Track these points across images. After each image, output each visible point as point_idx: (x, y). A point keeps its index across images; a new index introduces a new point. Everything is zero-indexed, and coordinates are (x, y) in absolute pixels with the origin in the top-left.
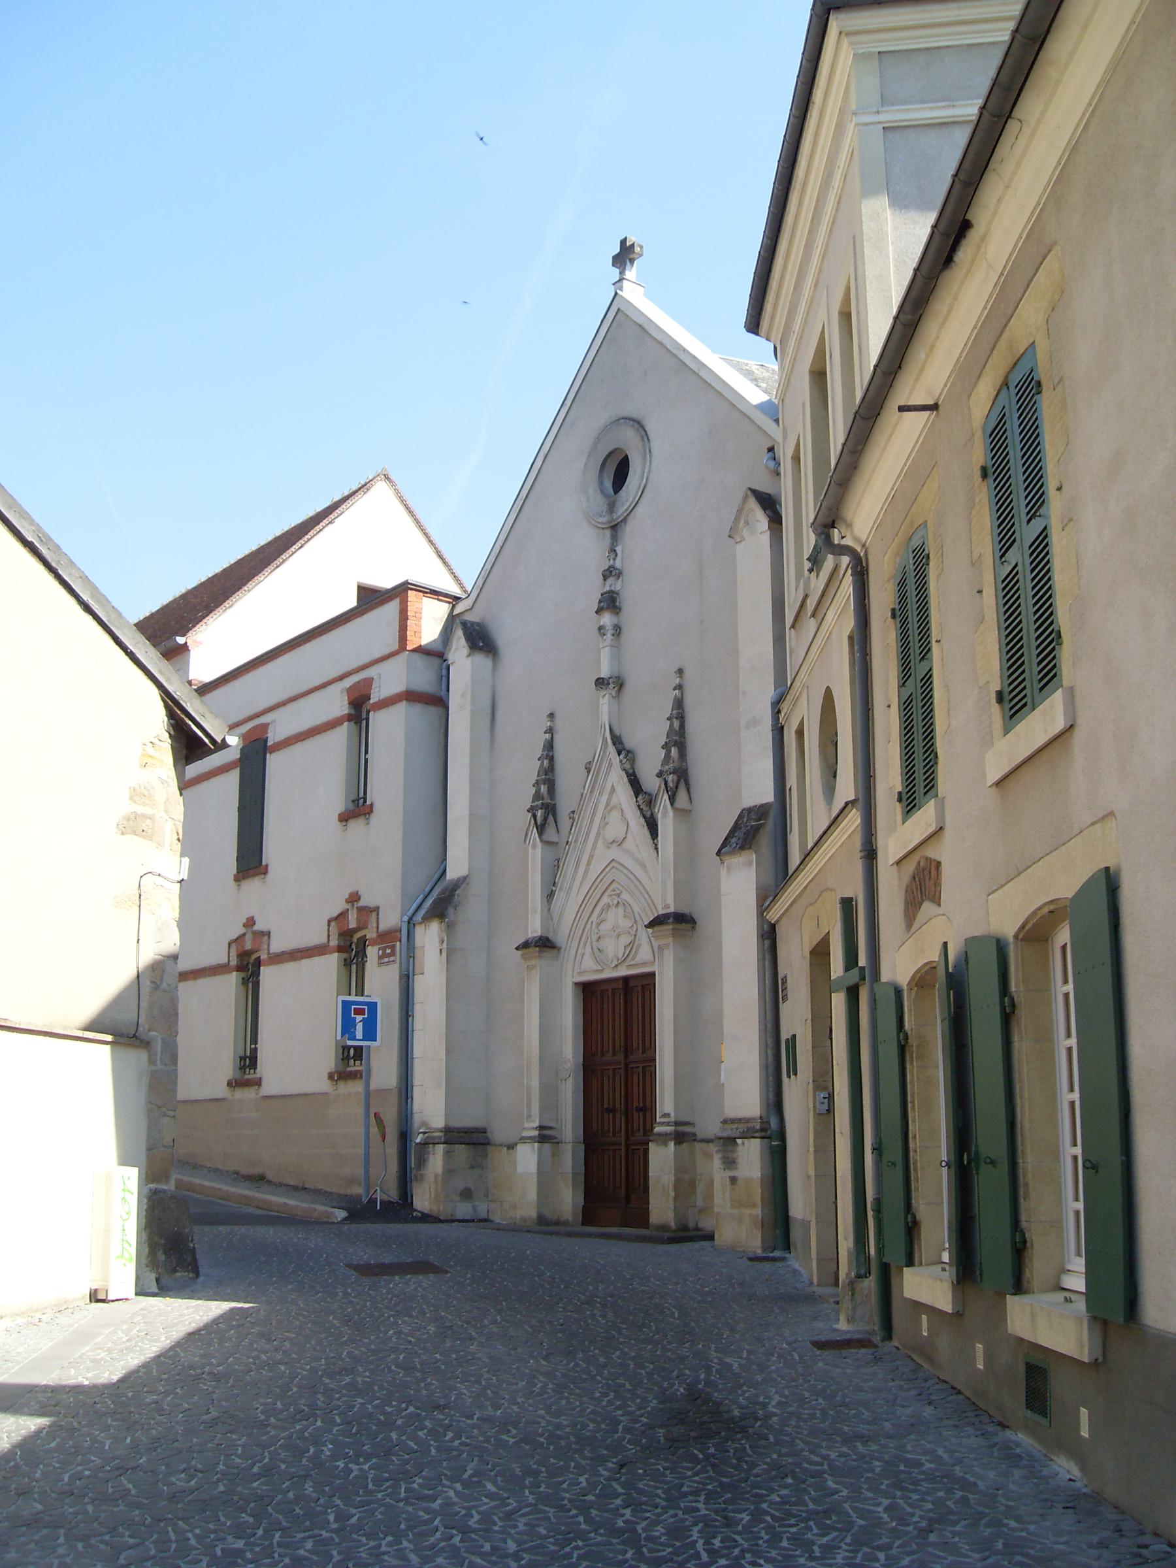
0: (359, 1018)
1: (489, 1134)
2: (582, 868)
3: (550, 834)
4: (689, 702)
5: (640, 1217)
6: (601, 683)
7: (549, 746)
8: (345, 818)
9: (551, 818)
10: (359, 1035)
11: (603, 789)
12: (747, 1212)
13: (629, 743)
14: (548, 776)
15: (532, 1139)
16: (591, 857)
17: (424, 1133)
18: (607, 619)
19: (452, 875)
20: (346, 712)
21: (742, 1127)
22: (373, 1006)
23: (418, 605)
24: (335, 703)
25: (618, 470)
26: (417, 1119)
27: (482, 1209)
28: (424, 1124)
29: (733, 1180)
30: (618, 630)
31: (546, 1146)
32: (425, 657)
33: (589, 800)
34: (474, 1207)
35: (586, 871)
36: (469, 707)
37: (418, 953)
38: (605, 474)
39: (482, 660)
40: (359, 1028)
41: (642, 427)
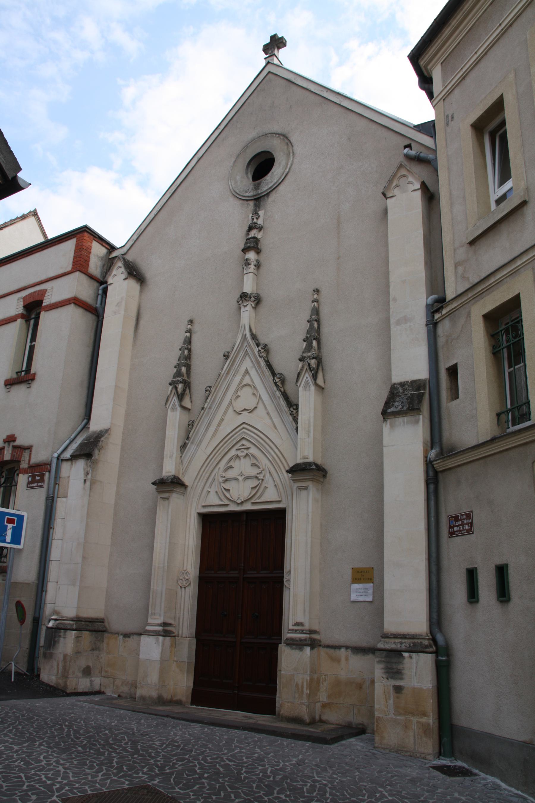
0: (10, 526)
1: (106, 624)
2: (212, 429)
3: (187, 403)
4: (324, 312)
5: (268, 706)
6: (244, 296)
7: (188, 341)
8: (10, 383)
9: (188, 390)
10: (8, 538)
11: (237, 372)
12: (415, 719)
13: (263, 340)
14: (186, 360)
15: (157, 634)
16: (222, 420)
17: (56, 620)
18: (251, 255)
19: (95, 426)
20: (21, 312)
21: (406, 643)
22: (21, 518)
23: (89, 244)
24: (14, 306)
25: (262, 165)
26: (48, 609)
27: (97, 682)
28: (55, 612)
29: (398, 689)
30: (258, 265)
31: (168, 639)
32: (89, 280)
33: (225, 379)
34: (91, 682)
35: (216, 431)
36: (122, 312)
37: (62, 482)
38: (249, 169)
39: (132, 284)
40: (9, 533)
41: (287, 138)
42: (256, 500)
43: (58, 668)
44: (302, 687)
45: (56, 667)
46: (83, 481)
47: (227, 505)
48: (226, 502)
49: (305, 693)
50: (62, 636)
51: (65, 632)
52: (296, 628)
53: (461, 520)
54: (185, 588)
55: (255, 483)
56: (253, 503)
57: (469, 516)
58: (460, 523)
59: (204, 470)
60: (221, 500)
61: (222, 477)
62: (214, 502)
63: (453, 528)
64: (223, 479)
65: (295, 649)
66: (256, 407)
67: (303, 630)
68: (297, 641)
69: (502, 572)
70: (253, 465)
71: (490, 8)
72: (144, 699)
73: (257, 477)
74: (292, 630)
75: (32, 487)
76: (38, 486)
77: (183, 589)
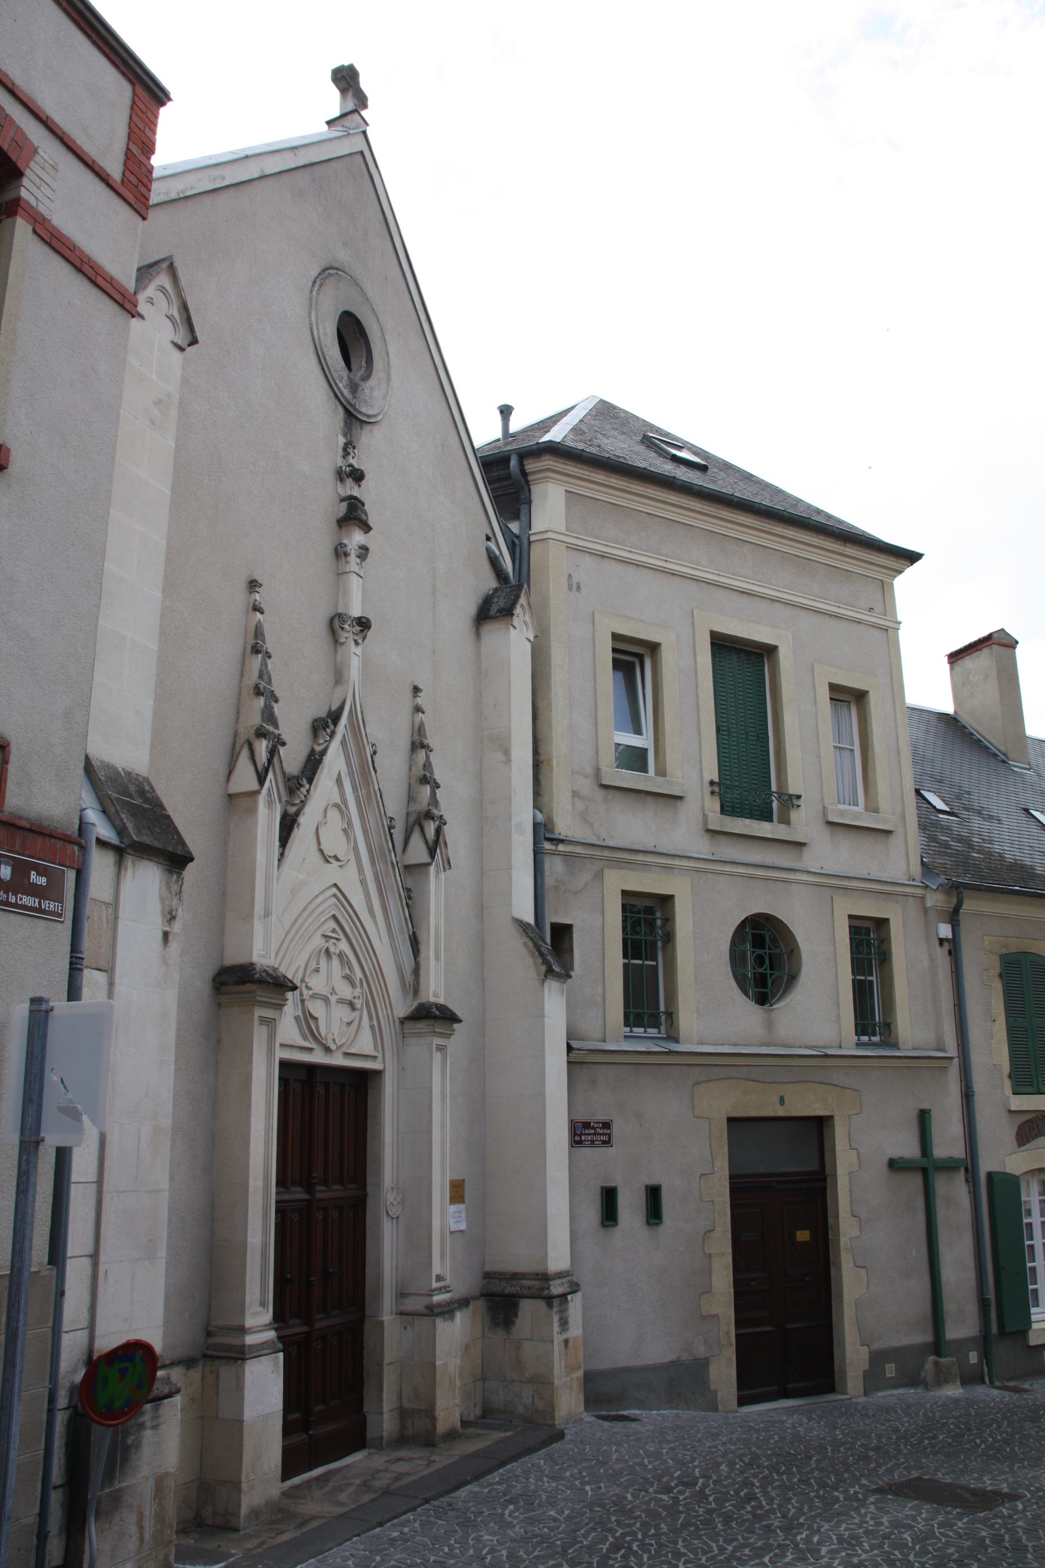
43: (141, 1528)
45: (134, 1530)
46: (160, 935)
50: (148, 1424)
51: (156, 1409)
53: (595, 1128)
57: (607, 1125)
58: (592, 1131)
60: (305, 1038)
63: (580, 1135)
69: (654, 1193)
71: (644, 515)
75: (16, 905)
76: (40, 910)
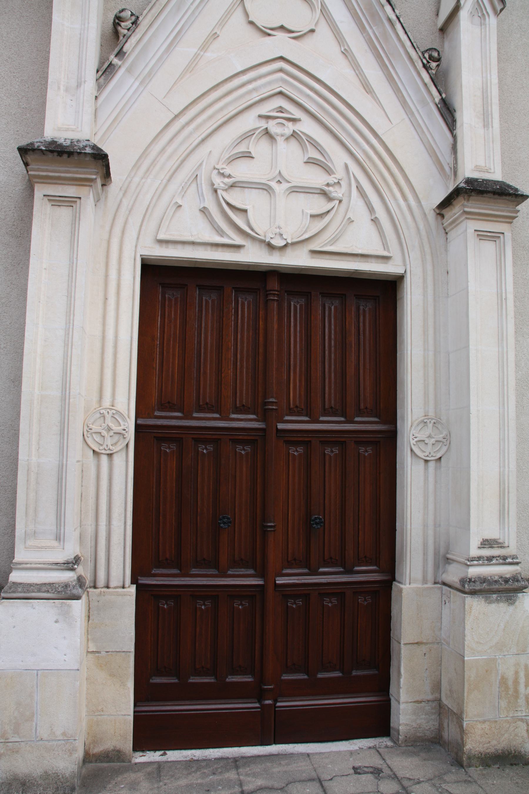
42: (325, 245)
44: (516, 682)
47: (238, 247)
48: (238, 240)
49: (521, 696)
52: (487, 552)
54: (110, 455)
55: (319, 205)
56: (315, 253)
59: (163, 150)
60: (220, 232)
61: (223, 175)
62: (193, 236)
64: (226, 180)
65: (497, 601)
66: (312, 31)
67: (505, 558)
68: (496, 582)
70: (311, 162)
72: (24, 784)
73: (324, 193)
74: (479, 558)
77: (104, 459)
